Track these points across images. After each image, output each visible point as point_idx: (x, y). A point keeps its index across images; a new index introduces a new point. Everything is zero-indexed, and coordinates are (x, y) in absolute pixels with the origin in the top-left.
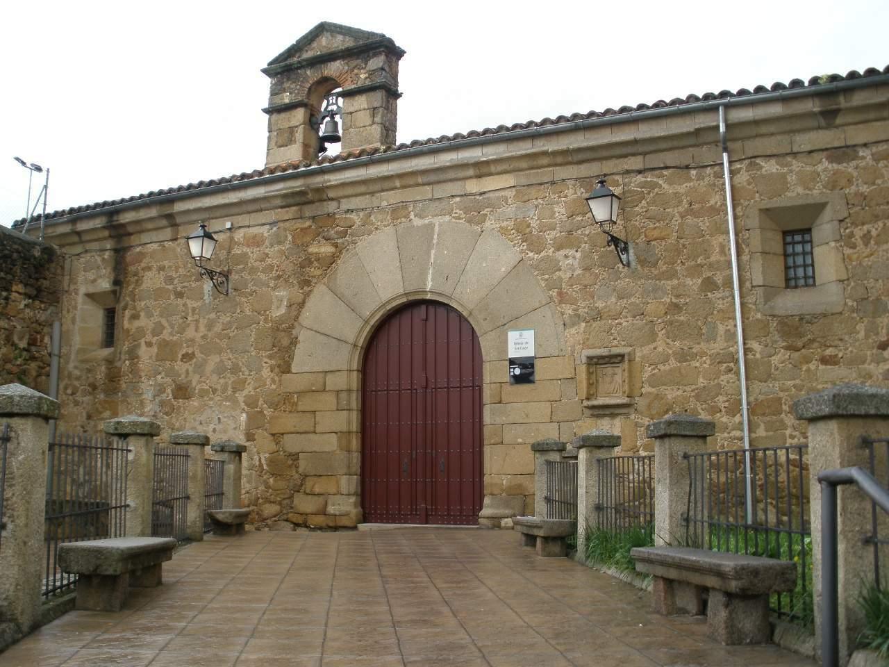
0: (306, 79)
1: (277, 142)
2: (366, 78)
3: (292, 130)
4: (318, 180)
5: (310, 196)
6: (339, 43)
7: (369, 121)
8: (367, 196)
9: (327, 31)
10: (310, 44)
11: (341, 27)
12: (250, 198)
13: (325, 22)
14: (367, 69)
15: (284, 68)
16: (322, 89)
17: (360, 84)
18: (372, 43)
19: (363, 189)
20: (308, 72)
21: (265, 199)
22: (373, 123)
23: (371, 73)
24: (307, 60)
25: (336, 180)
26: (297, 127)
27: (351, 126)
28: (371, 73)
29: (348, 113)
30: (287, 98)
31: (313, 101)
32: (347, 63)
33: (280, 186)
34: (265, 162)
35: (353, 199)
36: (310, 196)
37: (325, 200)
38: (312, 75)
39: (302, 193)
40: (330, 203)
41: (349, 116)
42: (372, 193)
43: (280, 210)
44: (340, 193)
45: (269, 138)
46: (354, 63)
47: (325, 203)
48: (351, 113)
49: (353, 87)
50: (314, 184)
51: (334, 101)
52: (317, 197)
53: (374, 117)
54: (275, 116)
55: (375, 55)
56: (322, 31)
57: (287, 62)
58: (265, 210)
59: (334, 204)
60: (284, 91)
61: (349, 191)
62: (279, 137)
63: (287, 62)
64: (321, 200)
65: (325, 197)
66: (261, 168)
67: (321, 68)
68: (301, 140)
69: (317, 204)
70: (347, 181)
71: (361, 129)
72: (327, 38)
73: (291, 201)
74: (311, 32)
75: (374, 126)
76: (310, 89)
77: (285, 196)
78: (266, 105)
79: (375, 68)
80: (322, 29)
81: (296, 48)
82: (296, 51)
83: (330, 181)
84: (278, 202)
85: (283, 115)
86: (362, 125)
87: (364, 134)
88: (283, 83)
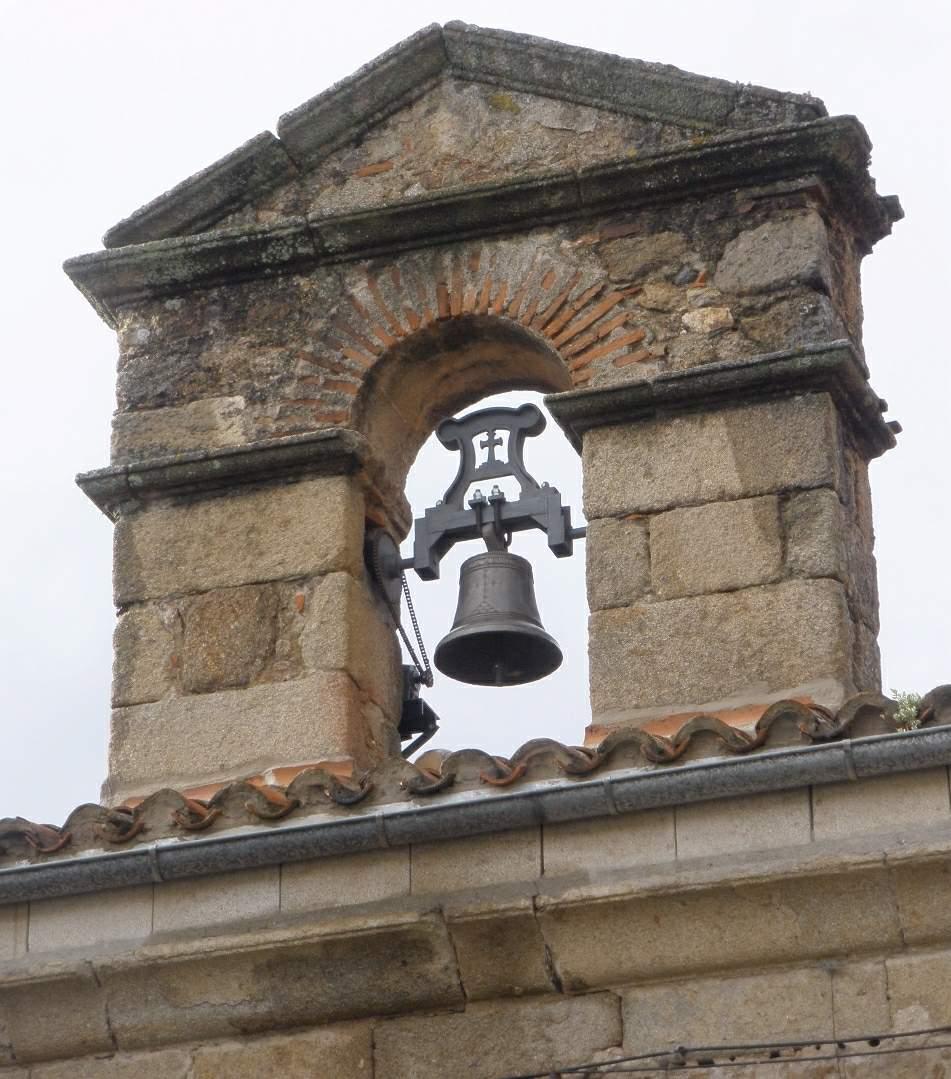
0: (345, 324)
1: (176, 663)
2: (719, 332)
3: (271, 600)
4: (504, 874)
5: (440, 968)
6: (537, 139)
7: (758, 560)
8: (801, 977)
9: (463, 79)
10: (358, 141)
11: (557, 57)
12: (54, 966)
13: (456, 29)
14: (725, 280)
15: (202, 266)
16: (421, 387)
17: (685, 359)
18: (750, 147)
19: (779, 929)
20: (360, 290)
21: (152, 975)
22: (787, 571)
23: (751, 306)
24: (352, 223)
25: (620, 874)
26: (303, 579)
27: (646, 587)
28: (751, 306)
29: (621, 516)
30: (230, 425)
31: (374, 441)
32: (597, 250)
33: (255, 900)
34: (104, 774)
35: (710, 994)
36: (440, 968)
37: (533, 993)
38: (382, 306)
39: (395, 946)
40: (559, 1008)
41: (633, 530)
42: (832, 960)
43: (232, 1047)
44: (639, 948)
45: (127, 642)
46: (644, 248)
47: (530, 1010)
48: (643, 515)
49: (648, 372)
50: (479, 893)
51: (502, 454)
52: (481, 972)
53: (784, 538)
54: (157, 522)
55: (765, 210)
56: (434, 75)
57: (234, 227)
58: (135, 1046)
59: (592, 1014)
60: (214, 381)
61: (690, 941)
62: (181, 639)
63: (234, 227)
64: (507, 994)
65: (535, 973)
66: (50, 812)
67: (435, 268)
68: (335, 657)
69: (477, 1014)
70: (693, 879)
71: (716, 603)
72: (461, 112)
73: (318, 992)
74: (373, 74)
75: (793, 589)
76: (370, 379)
77: (279, 963)
78: (100, 456)
79: (772, 276)
80: (436, 60)
81: (281, 157)
82: (279, 177)
83: (582, 878)
84: (232, 997)
85: (212, 515)
86: (716, 580)
87: (732, 628)
88: (202, 341)
